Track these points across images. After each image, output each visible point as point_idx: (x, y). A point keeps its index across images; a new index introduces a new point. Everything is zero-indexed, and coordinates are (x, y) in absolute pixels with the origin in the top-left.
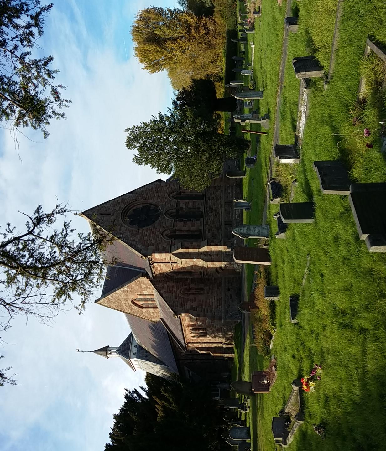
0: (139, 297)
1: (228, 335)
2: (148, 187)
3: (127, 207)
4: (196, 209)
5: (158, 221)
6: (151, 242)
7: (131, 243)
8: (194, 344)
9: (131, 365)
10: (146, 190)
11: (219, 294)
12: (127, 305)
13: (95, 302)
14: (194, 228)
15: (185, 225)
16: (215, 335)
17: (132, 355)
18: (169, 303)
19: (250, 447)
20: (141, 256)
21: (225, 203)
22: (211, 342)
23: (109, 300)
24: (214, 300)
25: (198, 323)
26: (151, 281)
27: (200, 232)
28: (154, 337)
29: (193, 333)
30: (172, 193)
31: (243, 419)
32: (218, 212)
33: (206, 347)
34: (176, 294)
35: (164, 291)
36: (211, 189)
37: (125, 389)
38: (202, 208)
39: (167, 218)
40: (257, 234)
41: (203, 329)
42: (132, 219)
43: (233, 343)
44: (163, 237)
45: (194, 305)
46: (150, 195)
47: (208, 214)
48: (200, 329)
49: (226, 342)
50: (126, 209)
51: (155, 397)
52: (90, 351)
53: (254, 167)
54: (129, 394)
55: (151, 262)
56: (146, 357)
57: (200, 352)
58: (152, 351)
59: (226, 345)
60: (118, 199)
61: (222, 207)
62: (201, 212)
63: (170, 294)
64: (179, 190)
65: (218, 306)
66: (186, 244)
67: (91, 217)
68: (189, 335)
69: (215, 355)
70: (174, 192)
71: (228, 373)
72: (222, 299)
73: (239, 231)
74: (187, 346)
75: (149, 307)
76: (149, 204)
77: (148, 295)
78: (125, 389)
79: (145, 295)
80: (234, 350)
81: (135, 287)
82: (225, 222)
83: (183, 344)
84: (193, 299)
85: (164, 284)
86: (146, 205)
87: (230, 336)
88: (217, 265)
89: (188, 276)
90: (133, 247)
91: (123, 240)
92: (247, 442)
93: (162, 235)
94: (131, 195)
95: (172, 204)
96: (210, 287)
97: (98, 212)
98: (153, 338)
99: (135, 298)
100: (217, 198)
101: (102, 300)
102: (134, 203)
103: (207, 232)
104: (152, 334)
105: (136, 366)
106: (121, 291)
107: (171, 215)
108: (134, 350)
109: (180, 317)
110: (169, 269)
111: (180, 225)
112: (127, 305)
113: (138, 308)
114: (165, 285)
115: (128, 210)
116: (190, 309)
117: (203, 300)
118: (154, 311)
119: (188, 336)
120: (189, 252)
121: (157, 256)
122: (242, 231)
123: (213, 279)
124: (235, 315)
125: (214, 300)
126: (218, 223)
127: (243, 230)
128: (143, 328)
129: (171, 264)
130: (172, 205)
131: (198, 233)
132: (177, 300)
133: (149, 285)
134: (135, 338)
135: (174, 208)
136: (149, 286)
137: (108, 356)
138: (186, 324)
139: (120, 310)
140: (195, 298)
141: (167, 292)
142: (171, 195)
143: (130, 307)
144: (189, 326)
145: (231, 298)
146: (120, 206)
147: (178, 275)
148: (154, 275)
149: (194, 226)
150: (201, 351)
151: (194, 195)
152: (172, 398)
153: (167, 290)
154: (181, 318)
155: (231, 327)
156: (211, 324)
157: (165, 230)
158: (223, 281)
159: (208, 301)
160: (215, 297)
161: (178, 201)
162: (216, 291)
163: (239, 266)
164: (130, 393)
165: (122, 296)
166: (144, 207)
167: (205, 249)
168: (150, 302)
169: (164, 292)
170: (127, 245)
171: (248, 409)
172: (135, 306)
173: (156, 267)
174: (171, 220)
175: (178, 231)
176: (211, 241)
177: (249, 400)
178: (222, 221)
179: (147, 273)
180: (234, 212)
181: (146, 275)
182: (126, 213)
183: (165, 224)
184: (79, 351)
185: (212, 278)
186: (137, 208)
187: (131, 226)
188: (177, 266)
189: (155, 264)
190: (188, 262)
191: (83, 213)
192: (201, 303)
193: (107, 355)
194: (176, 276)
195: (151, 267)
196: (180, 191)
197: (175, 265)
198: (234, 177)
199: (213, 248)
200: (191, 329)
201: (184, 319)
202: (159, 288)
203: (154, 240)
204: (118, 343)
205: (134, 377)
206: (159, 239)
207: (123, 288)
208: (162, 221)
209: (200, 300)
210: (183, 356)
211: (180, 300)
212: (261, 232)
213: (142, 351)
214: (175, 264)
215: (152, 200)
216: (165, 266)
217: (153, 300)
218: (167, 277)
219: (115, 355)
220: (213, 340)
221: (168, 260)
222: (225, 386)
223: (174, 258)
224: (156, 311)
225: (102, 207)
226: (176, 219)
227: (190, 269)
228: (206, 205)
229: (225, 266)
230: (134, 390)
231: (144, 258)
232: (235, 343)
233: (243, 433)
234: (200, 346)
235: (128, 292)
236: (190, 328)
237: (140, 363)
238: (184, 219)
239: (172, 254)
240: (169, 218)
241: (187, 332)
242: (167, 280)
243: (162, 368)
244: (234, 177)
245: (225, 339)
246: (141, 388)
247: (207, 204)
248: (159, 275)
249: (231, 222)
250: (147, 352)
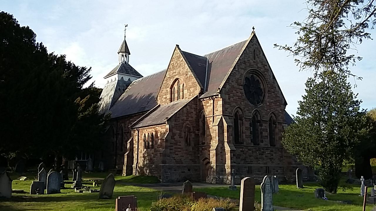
0: (181, 86)
1: (146, 170)
2: (279, 93)
3: (261, 74)
4: (261, 139)
5: (249, 103)
6: (231, 97)
7: (230, 79)
8: (137, 137)
9: (111, 74)
10: (277, 91)
11: (185, 161)
12: (174, 74)
13: (177, 45)
14: (244, 137)
15: (247, 129)
16: (146, 157)
17: (121, 76)
18: (178, 113)
19: (40, 193)
20: (220, 88)
21: (268, 167)
22: (139, 152)
23: (179, 57)
24: (181, 156)
25: (159, 141)
26: (197, 97)
28: (141, 98)
29: (148, 136)
31: (66, 185)
32: (259, 160)
33: (133, 148)
34: (186, 120)
35: (188, 109)
36: (280, 153)
37: (91, 68)
38: (262, 145)
39: (252, 112)
40: (265, 200)
41: (152, 145)
42: (250, 79)
43: (137, 174)
44: (236, 108)
45: (177, 137)
46: (272, 96)
48: (153, 142)
49: (139, 167)
50: (259, 73)
51: (88, 98)
52: (125, 37)
53: (316, 197)
54: (86, 71)
55: (214, 97)
56: (119, 89)
57: (129, 142)
58: (124, 95)
59: (135, 167)
61: (264, 164)
62: (259, 144)
63: (186, 114)
64: (278, 122)
65: (175, 159)
66: (231, 130)
67: (252, 42)
68: (147, 132)
69: (126, 157)
70: (276, 117)
71: (102, 169)
72: (181, 163)
73: (267, 182)
74: (136, 129)
75: (171, 94)
76: (264, 95)
77: (183, 94)
78: (91, 68)
79: (183, 91)
80: (130, 175)
81: (191, 82)
82: (251, 167)
83: (137, 126)
84: (181, 136)
86: (263, 92)
87: (145, 172)
88: (213, 159)
89: (201, 132)
90: (227, 81)
91: (233, 72)
92: (45, 190)
93: (237, 107)
94: (272, 77)
96: (191, 152)
97: (256, 48)
98: (139, 96)
99: (180, 82)
100: (272, 158)
101: (179, 52)
102: (265, 81)
103: (241, 149)
104: (143, 96)
105: (109, 79)
106: (187, 69)
107: (255, 115)
108: (126, 78)
109: (165, 123)
110: (207, 114)
111: (247, 124)
112: (174, 74)
113: (171, 84)
114: (193, 110)
115: (258, 75)
116: (173, 133)
117: (180, 145)
118: (168, 99)
119: (146, 130)
120: (224, 132)
121: (220, 102)
122: (267, 186)
123: (199, 155)
124: (167, 176)
125: (181, 156)
126: (249, 161)
127: (268, 187)
128: (149, 88)
129: (212, 116)
130: (264, 116)
131: (240, 141)
132: (181, 121)
133: (192, 95)
134: (138, 80)
135: (261, 117)
136: (191, 95)
137: (121, 53)
138: (158, 129)
139: (169, 67)
140: (182, 138)
141: (187, 112)
142: (273, 115)
143: (173, 77)
144: (156, 132)
145: (183, 172)
146: (262, 68)
147: (202, 122)
148: (202, 100)
150: (130, 143)
151: (274, 137)
152: (88, 114)
153: (189, 112)
154: (164, 125)
155: (154, 173)
156: (159, 153)
157: (242, 110)
158: (197, 164)
159: (179, 150)
160: (183, 156)
161: (268, 122)
162: (188, 158)
163: (212, 180)
164: (87, 72)
165: (182, 70)
166: (261, 90)
167: (227, 148)
168: (176, 95)
169: (188, 109)
170: (229, 75)
171: (78, 191)
172: (173, 82)
173: (209, 102)
174: (250, 115)
175: (241, 122)
176: (234, 153)
177: (90, 192)
178: (252, 164)
179: (203, 93)
180: (261, 176)
181: (201, 93)
182: (256, 73)
183: (247, 110)
184: (126, 26)
185: (199, 154)
186: (260, 83)
187: (245, 79)
188: (211, 121)
189: (212, 101)
190: (214, 131)
191: (255, 35)
192: (178, 143)
193: (121, 52)
194: (201, 120)
195: (210, 97)
196: (277, 123)
197: (212, 119)
198: (297, 176)
199: (228, 156)
200: (152, 133)
201: (163, 127)
202: (190, 104)
203: (234, 99)
204: (133, 62)
205: (102, 78)
206: (234, 104)
207: (190, 71)
208: (250, 108)
209: (180, 142)
210: (121, 125)
211: (180, 123)
212: (267, 204)
213: (125, 85)
214: (212, 120)
215: (268, 97)
216: (211, 110)
217: (178, 98)
218: (200, 112)
219: (121, 60)
220: (141, 155)
221: (216, 113)
222: (90, 166)
223: (218, 119)
224: (167, 101)
225: (260, 52)
226: (252, 121)
227: (208, 133)
228: (265, 148)
229: (212, 167)
230: (90, 77)
231: (219, 91)
232: (137, 177)
233: (54, 186)
234: (134, 142)
235: (186, 75)
236: (154, 133)
237: (113, 83)
238: (252, 128)
239: (222, 117)
240: (253, 114)
241: (150, 130)
242: (198, 111)
243: (107, 104)
244: (297, 176)
245: (142, 166)
246: (93, 83)
247: (266, 149)
248: (201, 105)
249: (251, 173)
250: (124, 90)
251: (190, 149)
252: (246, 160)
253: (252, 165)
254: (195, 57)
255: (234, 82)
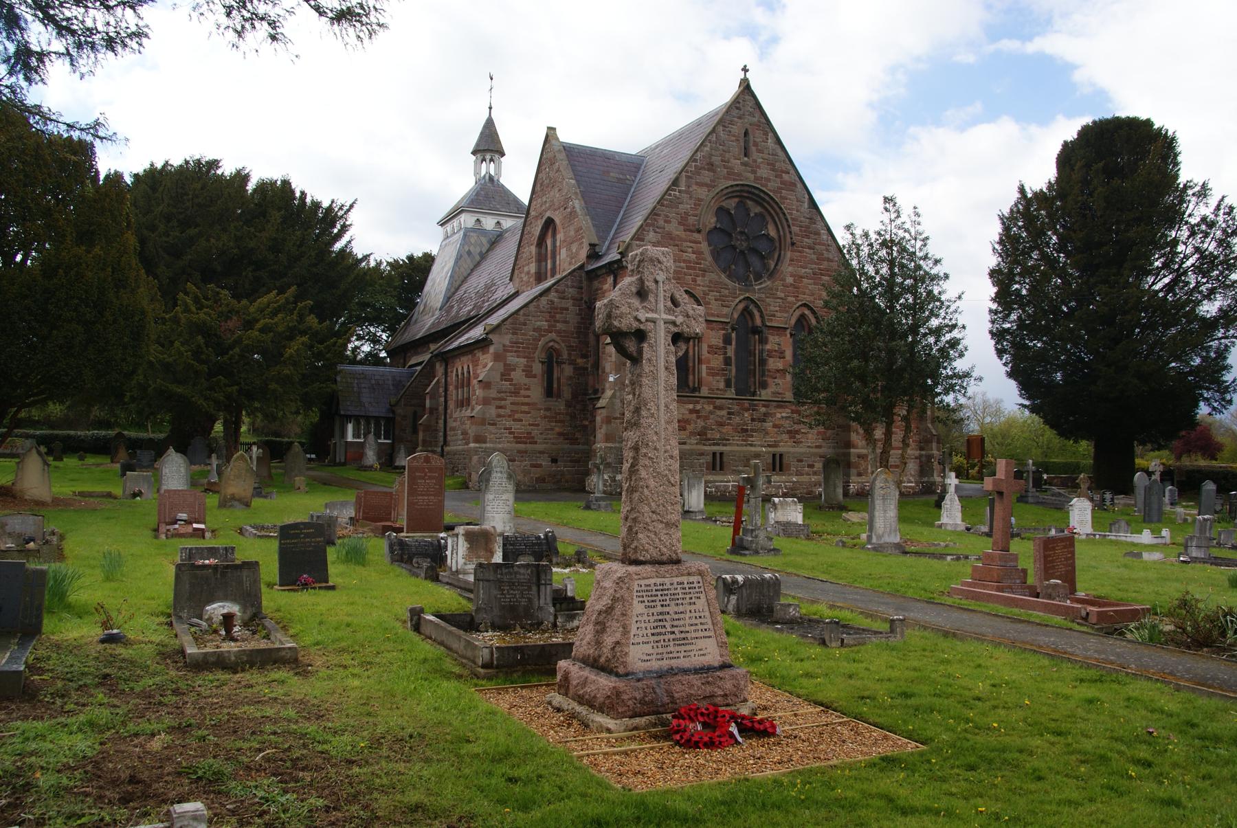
26: (582, 267)
27: (694, 390)
30: (814, 312)
39: (733, 305)
47: (747, 410)
60: (792, 171)
67: (738, 108)
85: (574, 299)
89: (591, 360)
94: (806, 205)
95: (778, 314)
100: (797, 432)
103: (691, 406)
105: (449, 227)
116: (505, 365)
131: (691, 384)
140: (535, 376)
142: (807, 312)
145: (533, 466)
149: (708, 374)
159: (526, 408)
178: (725, 445)
192: (523, 392)
209: (528, 389)
247: (778, 407)
251: (561, 406)
252: (705, 434)
253: (724, 448)
254: (1165, 158)
255: (674, 224)
